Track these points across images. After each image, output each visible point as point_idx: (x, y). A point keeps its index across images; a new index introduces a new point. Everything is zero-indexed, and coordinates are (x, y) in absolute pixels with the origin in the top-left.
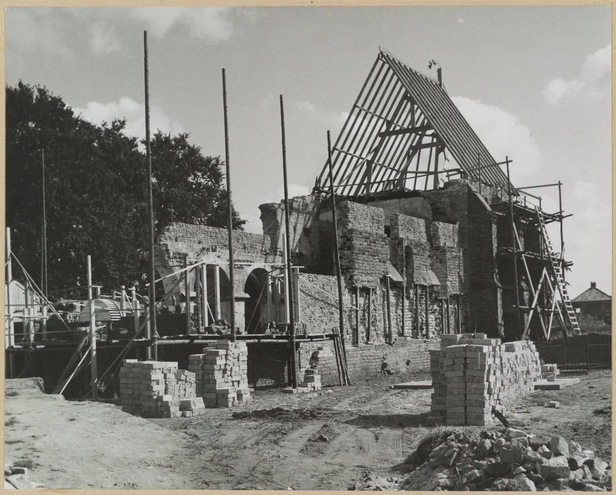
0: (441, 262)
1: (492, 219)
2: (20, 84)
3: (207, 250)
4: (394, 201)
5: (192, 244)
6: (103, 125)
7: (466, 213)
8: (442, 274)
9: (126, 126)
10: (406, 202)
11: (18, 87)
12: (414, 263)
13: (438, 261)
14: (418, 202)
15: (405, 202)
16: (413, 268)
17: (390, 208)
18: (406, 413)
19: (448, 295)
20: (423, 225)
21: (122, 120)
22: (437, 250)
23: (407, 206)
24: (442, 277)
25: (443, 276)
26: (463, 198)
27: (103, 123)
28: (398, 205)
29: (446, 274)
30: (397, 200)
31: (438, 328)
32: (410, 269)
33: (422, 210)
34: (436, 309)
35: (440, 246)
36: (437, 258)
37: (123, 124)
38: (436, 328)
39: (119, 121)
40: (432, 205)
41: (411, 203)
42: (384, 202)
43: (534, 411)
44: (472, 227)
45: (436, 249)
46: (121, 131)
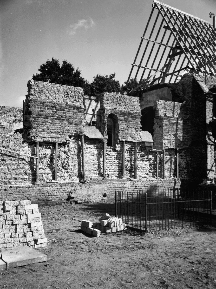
0: (160, 127)
1: (207, 98)
2: (53, 59)
3: (19, 121)
4: (155, 91)
5: (6, 117)
6: (106, 77)
7: (191, 95)
8: (160, 135)
9: (115, 76)
10: (160, 91)
11: (52, 60)
12: (119, 126)
13: (158, 126)
14: (165, 91)
15: (159, 91)
16: (118, 130)
17: (153, 95)
18: (98, 233)
19: (163, 148)
20: (136, 101)
21: (113, 74)
22: (158, 119)
23: (160, 93)
24: (160, 137)
25: (160, 136)
26: (190, 85)
27: (106, 76)
28: (156, 93)
29: (163, 135)
30: (156, 90)
31: (152, 171)
32: (116, 130)
33: (167, 95)
34: (151, 158)
35: (159, 116)
36: (158, 124)
37: (114, 75)
38: (150, 171)
39: (112, 74)
40: (172, 91)
41: (162, 91)
42: (150, 92)
43: (172, 258)
44: (195, 104)
45: (157, 118)
46: (113, 79)
